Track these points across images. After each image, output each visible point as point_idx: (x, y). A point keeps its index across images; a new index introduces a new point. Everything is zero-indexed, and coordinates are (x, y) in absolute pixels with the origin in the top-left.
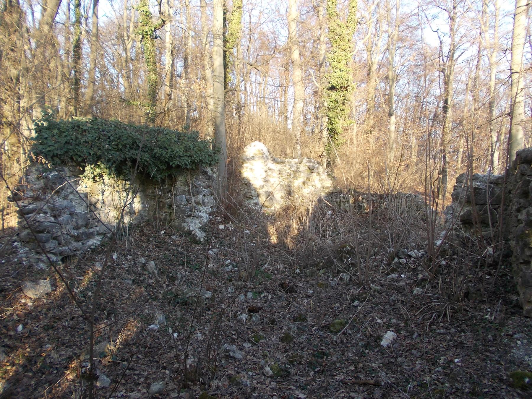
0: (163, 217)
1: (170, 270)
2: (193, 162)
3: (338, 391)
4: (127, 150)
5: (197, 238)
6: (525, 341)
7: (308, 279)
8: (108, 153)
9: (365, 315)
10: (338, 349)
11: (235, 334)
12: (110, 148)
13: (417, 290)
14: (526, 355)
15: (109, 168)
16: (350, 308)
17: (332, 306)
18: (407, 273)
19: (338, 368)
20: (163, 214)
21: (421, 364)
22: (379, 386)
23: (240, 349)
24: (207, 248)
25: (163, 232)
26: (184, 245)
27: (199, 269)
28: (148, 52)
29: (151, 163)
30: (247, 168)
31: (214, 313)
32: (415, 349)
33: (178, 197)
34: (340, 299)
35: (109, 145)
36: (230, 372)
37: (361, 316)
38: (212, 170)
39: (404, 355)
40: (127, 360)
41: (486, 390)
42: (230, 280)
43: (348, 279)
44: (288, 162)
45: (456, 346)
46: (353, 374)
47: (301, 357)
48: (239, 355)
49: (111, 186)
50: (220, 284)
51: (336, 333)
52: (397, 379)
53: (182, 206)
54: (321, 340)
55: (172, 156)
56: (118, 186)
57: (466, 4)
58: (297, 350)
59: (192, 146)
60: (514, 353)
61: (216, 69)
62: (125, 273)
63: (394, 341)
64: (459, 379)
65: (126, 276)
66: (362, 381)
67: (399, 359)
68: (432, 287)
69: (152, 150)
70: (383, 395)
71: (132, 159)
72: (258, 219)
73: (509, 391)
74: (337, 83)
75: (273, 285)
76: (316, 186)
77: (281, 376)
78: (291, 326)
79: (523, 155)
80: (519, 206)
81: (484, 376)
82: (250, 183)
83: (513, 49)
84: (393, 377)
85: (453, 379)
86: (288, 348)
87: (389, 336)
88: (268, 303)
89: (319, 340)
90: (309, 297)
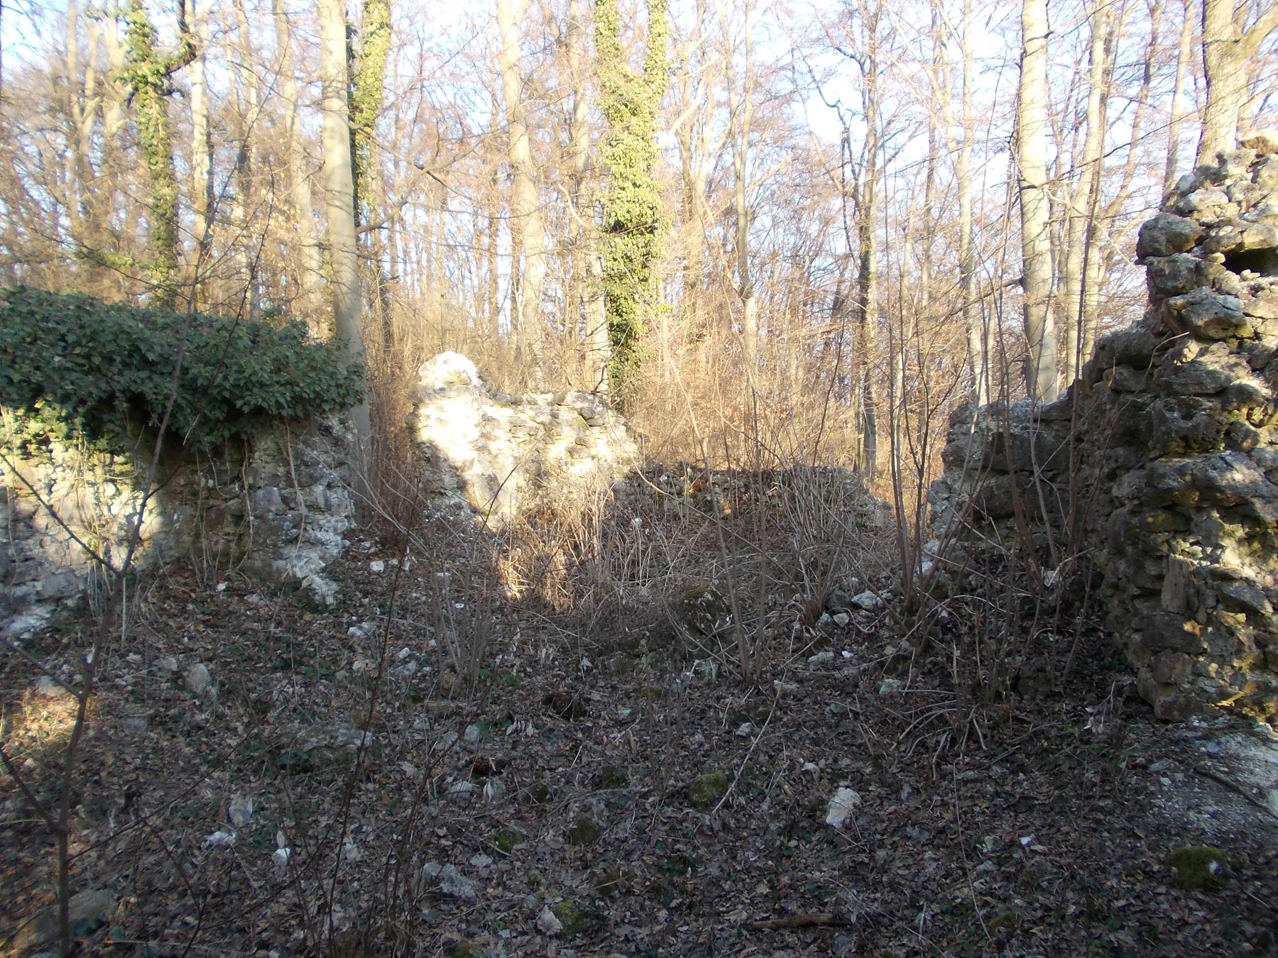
0: (220, 547)
1: (251, 685)
2: (297, 400)
3: (740, 951)
4: (115, 370)
5: (317, 598)
6: (1180, 776)
7: (615, 680)
8: (62, 378)
9: (771, 757)
10: (719, 847)
11: (445, 836)
12: (69, 365)
13: (889, 684)
14: (1189, 808)
15: (67, 419)
16: (731, 742)
17: (686, 741)
18: (855, 647)
19: (728, 892)
20: (216, 541)
21: (935, 860)
22: (843, 926)
23: (464, 873)
24: (345, 620)
25: (221, 587)
26: (283, 616)
27: (329, 676)
28: (151, 130)
29: (184, 403)
30: (428, 417)
31: (383, 786)
32: (913, 825)
33: (260, 493)
34: (703, 722)
35: (64, 356)
36: (448, 935)
37: (763, 758)
38: (342, 422)
39: (888, 842)
40: (155, 935)
41: (1122, 903)
42: (417, 699)
43: (714, 672)
44: (529, 403)
45: (1014, 805)
46: (769, 905)
47: (629, 876)
48: (467, 888)
49: (72, 468)
50: (389, 710)
51: (707, 807)
52: (884, 902)
53: (271, 516)
54: (673, 829)
55: (242, 383)
56: (92, 469)
57: (895, 46)
58: (615, 861)
59: (293, 359)
60: (1160, 807)
61: (332, 173)
62: (127, 700)
63: (858, 811)
64: (1045, 884)
65: (131, 707)
66: (796, 921)
67: (881, 854)
68: (923, 673)
69: (185, 370)
70: (861, 949)
71: (129, 395)
72: (468, 546)
73: (1177, 899)
74: (627, 216)
75: (528, 703)
76: (594, 461)
77: (585, 931)
78: (590, 799)
79: (1119, 346)
80: (1114, 465)
81: (1104, 871)
82: (438, 457)
83: (1024, 134)
84: (875, 900)
85: (1031, 886)
86: (589, 856)
87: (842, 803)
88: (521, 748)
89: (666, 828)
90: (621, 724)
